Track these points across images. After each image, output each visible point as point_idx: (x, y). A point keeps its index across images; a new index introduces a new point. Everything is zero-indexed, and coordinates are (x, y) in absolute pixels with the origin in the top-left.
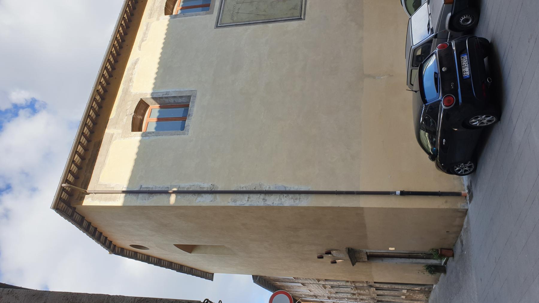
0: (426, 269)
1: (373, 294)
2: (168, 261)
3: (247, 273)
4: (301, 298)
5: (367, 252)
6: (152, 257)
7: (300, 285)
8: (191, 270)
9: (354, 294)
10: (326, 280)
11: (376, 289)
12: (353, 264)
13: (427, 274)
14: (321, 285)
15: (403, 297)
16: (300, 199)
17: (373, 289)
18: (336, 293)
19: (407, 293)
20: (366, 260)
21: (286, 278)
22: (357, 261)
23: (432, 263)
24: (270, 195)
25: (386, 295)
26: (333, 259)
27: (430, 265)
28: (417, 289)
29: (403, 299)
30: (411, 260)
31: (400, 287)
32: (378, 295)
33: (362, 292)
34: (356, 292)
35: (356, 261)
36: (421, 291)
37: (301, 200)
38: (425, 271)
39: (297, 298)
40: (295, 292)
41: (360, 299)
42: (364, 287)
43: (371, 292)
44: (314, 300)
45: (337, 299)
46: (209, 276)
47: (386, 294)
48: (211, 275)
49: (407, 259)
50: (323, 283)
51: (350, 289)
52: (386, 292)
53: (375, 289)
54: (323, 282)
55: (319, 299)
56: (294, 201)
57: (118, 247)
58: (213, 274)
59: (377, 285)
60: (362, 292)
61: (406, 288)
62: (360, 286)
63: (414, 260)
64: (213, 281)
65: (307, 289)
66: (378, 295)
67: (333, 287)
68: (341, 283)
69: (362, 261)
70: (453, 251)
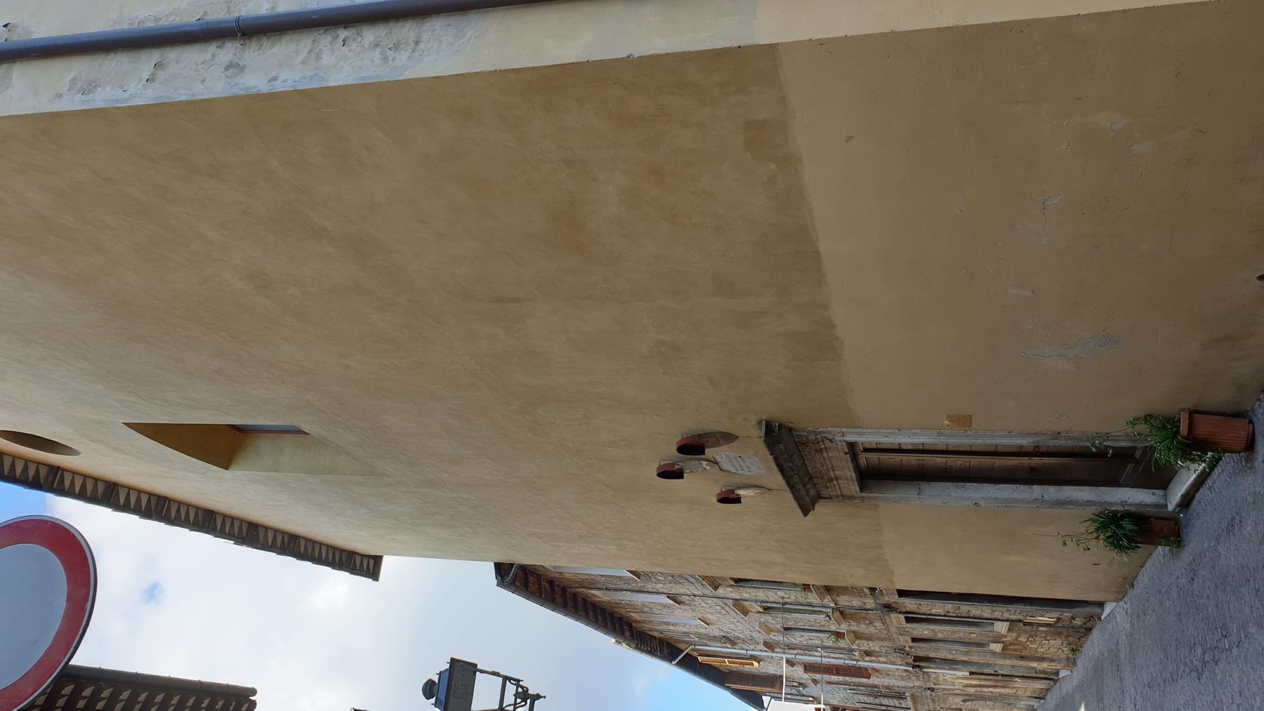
0: (1097, 530)
1: (901, 635)
2: (198, 508)
3: (472, 554)
4: (691, 645)
5: (852, 446)
6: (129, 488)
7: (665, 600)
8: (289, 542)
9: (839, 635)
10: (739, 581)
11: (908, 620)
12: (806, 511)
13: (1101, 551)
14: (730, 602)
15: (997, 647)
16: (417, 43)
17: (897, 619)
18: (786, 629)
19: (1010, 634)
20: (854, 488)
21: (611, 576)
22: (819, 497)
23: (1123, 503)
24: (265, 42)
25: (939, 641)
26: (725, 487)
27: (1115, 513)
28: (1045, 619)
29: (993, 653)
30: (1037, 490)
31: (985, 611)
32: (914, 640)
33: (862, 628)
34: (844, 628)
35: (812, 492)
36: (1054, 629)
37: (421, 46)
38: (1090, 537)
39: (681, 646)
40: (665, 627)
41: (860, 651)
42: (865, 609)
43: (893, 629)
44: (736, 654)
45: (795, 652)
46: (367, 566)
47: (940, 636)
48: (372, 562)
49: (1022, 487)
50: (733, 593)
51: (824, 616)
52: (941, 631)
53: (902, 617)
54: (731, 592)
55: (743, 649)
56: (385, 59)
57: (38, 463)
58: (378, 560)
59: (910, 604)
60: (862, 628)
61: (1007, 615)
62: (852, 608)
63: (1051, 492)
64: (377, 580)
65: (694, 614)
66: (914, 640)
67: (769, 608)
68: (793, 596)
69: (837, 496)
70: (1251, 422)
